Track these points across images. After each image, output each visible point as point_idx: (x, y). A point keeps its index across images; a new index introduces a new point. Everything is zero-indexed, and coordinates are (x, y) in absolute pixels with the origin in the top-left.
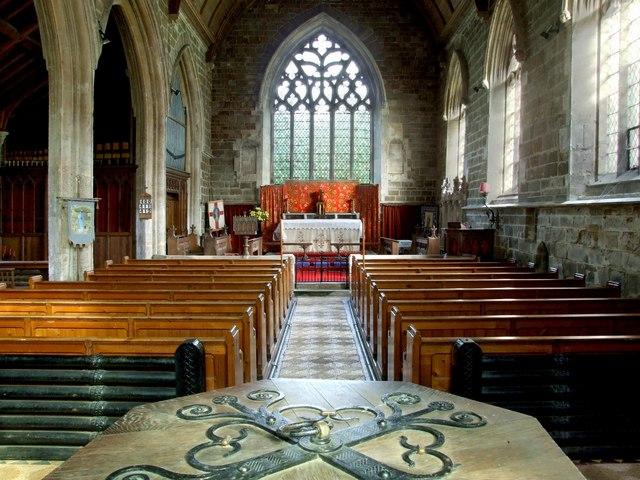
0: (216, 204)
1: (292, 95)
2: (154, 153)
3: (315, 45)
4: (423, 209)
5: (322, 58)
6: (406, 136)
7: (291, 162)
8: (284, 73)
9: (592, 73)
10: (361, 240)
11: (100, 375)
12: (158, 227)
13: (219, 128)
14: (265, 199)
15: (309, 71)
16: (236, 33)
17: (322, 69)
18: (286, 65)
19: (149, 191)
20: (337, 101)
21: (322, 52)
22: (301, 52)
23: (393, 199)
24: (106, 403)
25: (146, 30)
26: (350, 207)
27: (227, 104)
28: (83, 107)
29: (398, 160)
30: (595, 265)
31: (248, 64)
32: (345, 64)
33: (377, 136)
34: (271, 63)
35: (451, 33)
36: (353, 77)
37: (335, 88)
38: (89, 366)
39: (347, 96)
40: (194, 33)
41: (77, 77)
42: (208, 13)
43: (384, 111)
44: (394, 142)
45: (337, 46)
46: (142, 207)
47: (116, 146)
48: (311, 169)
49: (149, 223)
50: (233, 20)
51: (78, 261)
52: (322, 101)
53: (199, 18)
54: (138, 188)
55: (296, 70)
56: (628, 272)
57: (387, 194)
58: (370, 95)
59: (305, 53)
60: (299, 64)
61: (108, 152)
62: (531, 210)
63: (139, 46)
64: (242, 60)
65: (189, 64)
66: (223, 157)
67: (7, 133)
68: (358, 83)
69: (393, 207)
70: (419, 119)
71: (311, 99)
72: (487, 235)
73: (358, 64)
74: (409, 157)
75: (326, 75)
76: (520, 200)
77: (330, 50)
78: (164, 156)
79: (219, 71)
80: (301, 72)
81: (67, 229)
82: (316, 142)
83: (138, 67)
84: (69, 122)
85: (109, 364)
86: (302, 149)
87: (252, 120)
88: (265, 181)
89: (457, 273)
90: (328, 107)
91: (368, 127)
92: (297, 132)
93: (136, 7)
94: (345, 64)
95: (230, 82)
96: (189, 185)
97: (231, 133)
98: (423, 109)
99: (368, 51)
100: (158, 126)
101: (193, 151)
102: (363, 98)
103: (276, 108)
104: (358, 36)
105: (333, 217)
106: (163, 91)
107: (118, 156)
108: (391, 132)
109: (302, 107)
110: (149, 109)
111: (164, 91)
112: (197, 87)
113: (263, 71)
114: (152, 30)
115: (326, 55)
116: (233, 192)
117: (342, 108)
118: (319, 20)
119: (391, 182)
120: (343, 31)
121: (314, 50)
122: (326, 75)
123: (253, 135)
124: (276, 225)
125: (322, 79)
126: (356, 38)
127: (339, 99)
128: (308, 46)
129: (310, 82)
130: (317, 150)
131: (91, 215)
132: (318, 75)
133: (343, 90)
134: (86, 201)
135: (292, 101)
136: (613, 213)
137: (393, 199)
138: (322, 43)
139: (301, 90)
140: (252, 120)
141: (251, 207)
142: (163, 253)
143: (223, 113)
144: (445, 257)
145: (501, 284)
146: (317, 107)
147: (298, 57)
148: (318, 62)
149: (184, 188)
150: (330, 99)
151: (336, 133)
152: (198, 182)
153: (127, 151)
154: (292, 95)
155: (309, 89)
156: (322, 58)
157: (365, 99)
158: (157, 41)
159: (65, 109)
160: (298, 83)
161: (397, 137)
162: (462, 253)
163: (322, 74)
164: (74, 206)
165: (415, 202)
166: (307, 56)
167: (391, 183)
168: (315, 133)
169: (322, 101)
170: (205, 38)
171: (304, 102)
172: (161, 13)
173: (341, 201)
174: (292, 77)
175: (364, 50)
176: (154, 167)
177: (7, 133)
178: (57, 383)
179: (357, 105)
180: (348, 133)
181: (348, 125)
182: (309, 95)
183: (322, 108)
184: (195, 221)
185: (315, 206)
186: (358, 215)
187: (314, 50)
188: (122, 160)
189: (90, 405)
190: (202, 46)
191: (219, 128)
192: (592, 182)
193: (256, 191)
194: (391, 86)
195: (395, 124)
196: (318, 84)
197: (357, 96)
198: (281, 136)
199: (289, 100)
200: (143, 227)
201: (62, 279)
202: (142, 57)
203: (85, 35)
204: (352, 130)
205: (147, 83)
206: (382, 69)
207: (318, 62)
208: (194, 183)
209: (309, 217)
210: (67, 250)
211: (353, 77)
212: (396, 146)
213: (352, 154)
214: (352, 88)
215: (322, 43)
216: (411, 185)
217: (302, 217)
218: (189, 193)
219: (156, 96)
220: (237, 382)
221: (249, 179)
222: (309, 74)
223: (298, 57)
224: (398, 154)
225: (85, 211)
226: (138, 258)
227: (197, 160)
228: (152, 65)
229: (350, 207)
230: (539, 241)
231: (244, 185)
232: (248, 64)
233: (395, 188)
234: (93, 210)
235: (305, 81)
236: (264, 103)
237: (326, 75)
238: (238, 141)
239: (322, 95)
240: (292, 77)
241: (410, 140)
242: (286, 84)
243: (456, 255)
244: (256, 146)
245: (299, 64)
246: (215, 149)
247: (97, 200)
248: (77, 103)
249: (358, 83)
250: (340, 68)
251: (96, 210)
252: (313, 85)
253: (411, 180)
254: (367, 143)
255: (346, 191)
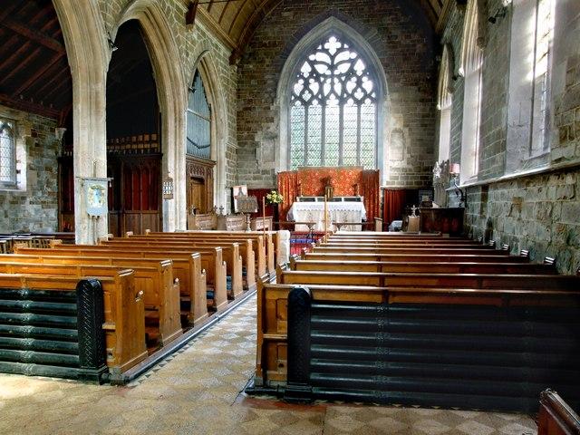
0: (240, 189)
1: (307, 92)
2: (175, 143)
3: (327, 46)
4: (420, 192)
5: (333, 58)
6: (406, 125)
7: (306, 150)
8: (299, 72)
9: (529, 52)
10: (363, 221)
11: (27, 304)
12: (180, 207)
13: (242, 123)
14: (282, 184)
15: (321, 69)
16: (257, 39)
17: (332, 67)
18: (301, 65)
19: (171, 175)
20: (345, 95)
21: (332, 52)
22: (315, 53)
23: (393, 183)
24: (33, 327)
25: (164, 39)
26: (355, 191)
27: (250, 101)
28: (97, 104)
29: (398, 148)
30: (518, 236)
31: (268, 66)
32: (353, 62)
33: (380, 126)
34: (286, 64)
35: (442, 31)
36: (359, 73)
37: (344, 84)
38: (17, 296)
39: (355, 90)
40: (215, 40)
41: (92, 78)
42: (227, 22)
43: (387, 103)
44: (396, 131)
45: (346, 46)
46: (166, 189)
47: (147, 138)
48: (322, 157)
49: (171, 203)
50: (253, 27)
51: (95, 231)
52: (332, 96)
53: (217, 26)
54: (163, 173)
55: (310, 70)
56: (537, 241)
57: (389, 180)
58: (375, 89)
59: (319, 54)
60: (312, 63)
61: (141, 142)
62: (485, 187)
63: (159, 52)
64: (262, 62)
65: (210, 66)
66: (246, 147)
67: (65, 129)
68: (365, 79)
69: (394, 191)
70: (418, 110)
71: (322, 94)
72: (459, 213)
73: (365, 61)
74: (408, 144)
75: (336, 72)
76: (479, 180)
77: (339, 50)
78: (185, 142)
79: (242, 73)
80: (314, 71)
81: (85, 203)
82: (327, 133)
83: (159, 72)
84: (85, 115)
85: (33, 296)
86: (314, 140)
87: (271, 114)
88: (281, 167)
89: (436, 248)
90: (337, 101)
91: (373, 118)
92: (310, 124)
93: (152, 19)
94: (353, 62)
95: (253, 82)
96: (215, 173)
97: (253, 126)
98: (422, 101)
99: (371, 49)
100: (179, 120)
101: (219, 142)
102: (368, 92)
103: (292, 103)
104: (363, 36)
105: (339, 200)
106: (182, 90)
107: (149, 146)
108: (393, 122)
109: (315, 102)
110: (170, 106)
111: (183, 90)
112: (220, 87)
113: (280, 71)
114: (168, 38)
115: (336, 55)
116: (255, 178)
117: (351, 101)
118: (330, 22)
119: (392, 169)
120: (350, 33)
121: (326, 51)
122: (336, 72)
123: (272, 127)
124: (289, 207)
125: (332, 76)
126: (361, 37)
127: (347, 93)
128: (320, 48)
129: (322, 79)
130: (328, 140)
131: (105, 192)
132: (329, 73)
133: (351, 85)
134: (101, 180)
135: (307, 96)
136: (532, 185)
137: (393, 183)
138: (333, 44)
139: (314, 86)
140: (271, 114)
141: (269, 191)
142: (184, 229)
143: (246, 109)
144: (420, 234)
145: (467, 257)
146: (328, 102)
147: (312, 57)
148: (329, 61)
149: (210, 174)
150: (339, 94)
151: (345, 124)
152: (223, 169)
153: (155, 142)
154: (307, 92)
155: (321, 85)
156: (333, 58)
157: (371, 93)
158: (174, 48)
159: (82, 105)
160: (312, 81)
161: (398, 126)
162: (433, 230)
163: (332, 72)
164: (89, 184)
165: (414, 186)
166: (320, 56)
167: (392, 169)
168: (327, 125)
169: (332, 96)
170: (227, 44)
171: (316, 97)
172: (178, 24)
173: (347, 185)
174: (306, 75)
175: (368, 48)
176: (175, 154)
177: (65, 129)
178: (47, 326)
179: (363, 99)
180: (355, 124)
181: (355, 117)
182: (321, 91)
183: (333, 102)
184: (221, 201)
185: (324, 187)
186: (362, 198)
187: (326, 51)
188: (152, 149)
189: (21, 328)
190: (224, 52)
191: (242, 123)
192: (526, 157)
193: (274, 177)
194: (393, 80)
195: (396, 115)
196: (329, 81)
197: (364, 90)
198: (297, 129)
199: (304, 96)
200: (167, 206)
201: (82, 243)
202: (161, 61)
203: (97, 43)
204: (359, 121)
205: (168, 83)
206: (386, 66)
207: (329, 61)
208: (219, 172)
209: (320, 200)
210: (86, 221)
211: (359, 73)
212: (397, 135)
213: (358, 143)
214: (359, 83)
215: (333, 44)
216: (410, 170)
217: (313, 200)
218: (215, 178)
219: (176, 94)
220: (156, 316)
221: (268, 166)
222: (321, 72)
223: (312, 57)
224: (398, 142)
225: (100, 189)
226: (164, 231)
227: (222, 148)
228: (171, 68)
229: (355, 191)
230: (488, 217)
231: (265, 172)
232: (268, 66)
233: (396, 173)
234: (107, 188)
235: (317, 79)
236: (281, 100)
237: (336, 72)
238: (259, 133)
239: (332, 91)
240: (306, 75)
241: (410, 130)
242: (301, 81)
243: (428, 232)
244: (274, 137)
245: (312, 63)
246: (241, 141)
247: (110, 179)
248: (92, 100)
249: (365, 79)
250: (348, 65)
251: (109, 187)
252: (325, 81)
253: (410, 166)
254: (373, 132)
255: (353, 175)
